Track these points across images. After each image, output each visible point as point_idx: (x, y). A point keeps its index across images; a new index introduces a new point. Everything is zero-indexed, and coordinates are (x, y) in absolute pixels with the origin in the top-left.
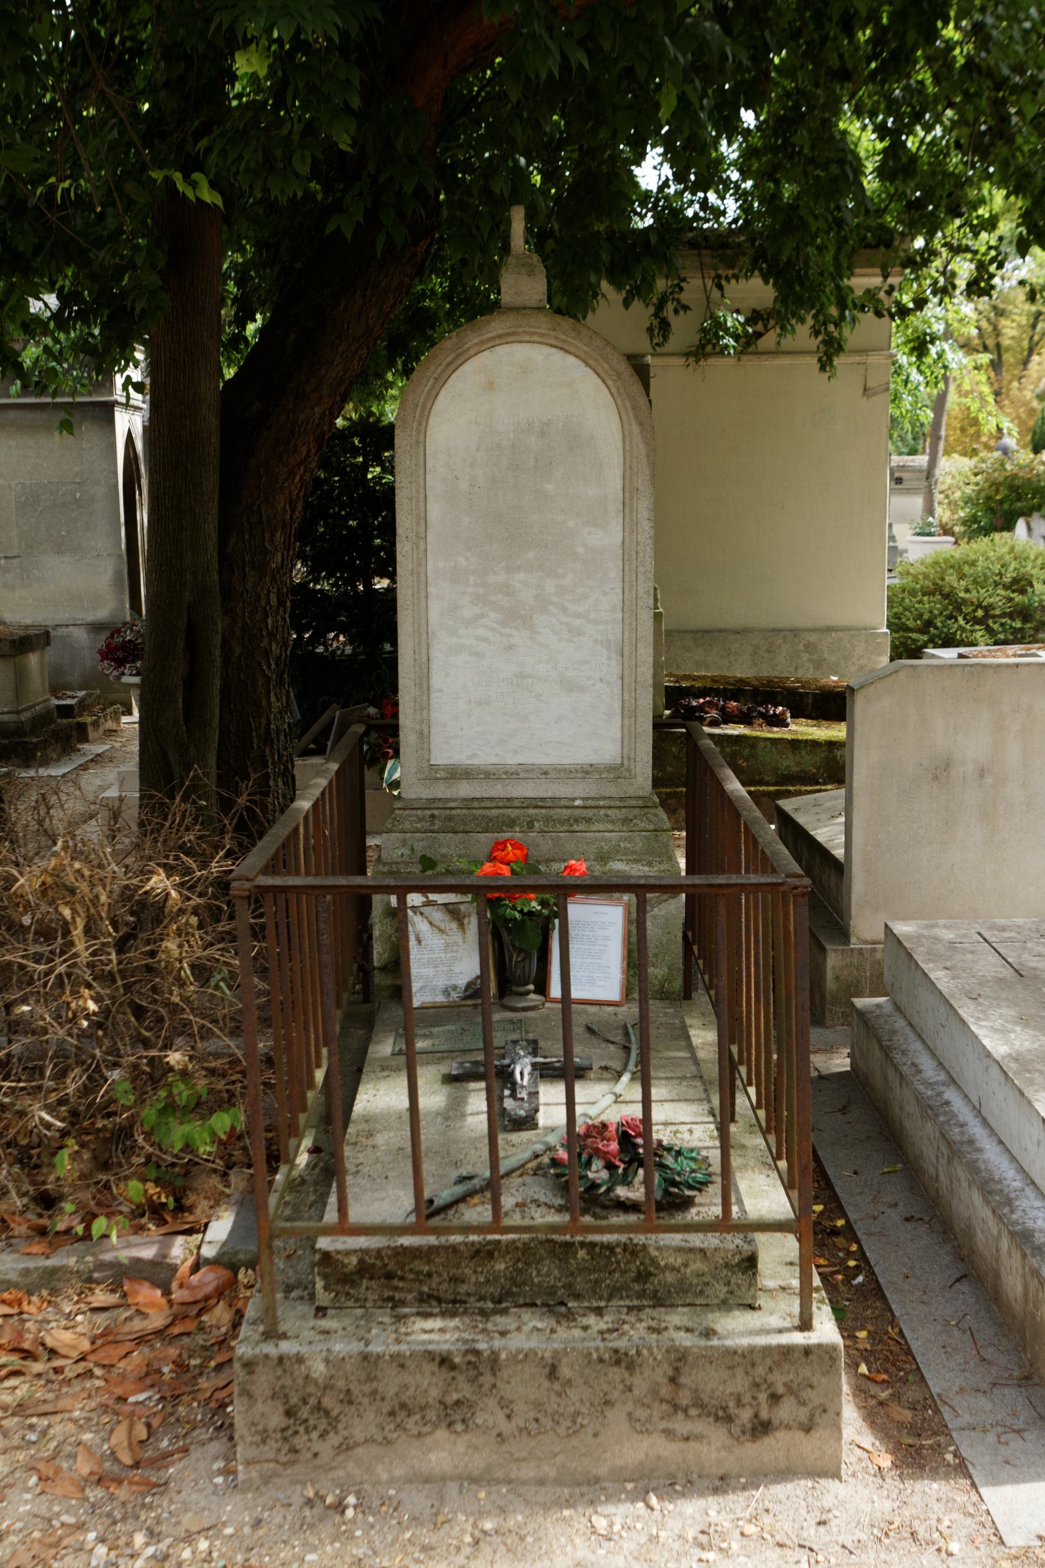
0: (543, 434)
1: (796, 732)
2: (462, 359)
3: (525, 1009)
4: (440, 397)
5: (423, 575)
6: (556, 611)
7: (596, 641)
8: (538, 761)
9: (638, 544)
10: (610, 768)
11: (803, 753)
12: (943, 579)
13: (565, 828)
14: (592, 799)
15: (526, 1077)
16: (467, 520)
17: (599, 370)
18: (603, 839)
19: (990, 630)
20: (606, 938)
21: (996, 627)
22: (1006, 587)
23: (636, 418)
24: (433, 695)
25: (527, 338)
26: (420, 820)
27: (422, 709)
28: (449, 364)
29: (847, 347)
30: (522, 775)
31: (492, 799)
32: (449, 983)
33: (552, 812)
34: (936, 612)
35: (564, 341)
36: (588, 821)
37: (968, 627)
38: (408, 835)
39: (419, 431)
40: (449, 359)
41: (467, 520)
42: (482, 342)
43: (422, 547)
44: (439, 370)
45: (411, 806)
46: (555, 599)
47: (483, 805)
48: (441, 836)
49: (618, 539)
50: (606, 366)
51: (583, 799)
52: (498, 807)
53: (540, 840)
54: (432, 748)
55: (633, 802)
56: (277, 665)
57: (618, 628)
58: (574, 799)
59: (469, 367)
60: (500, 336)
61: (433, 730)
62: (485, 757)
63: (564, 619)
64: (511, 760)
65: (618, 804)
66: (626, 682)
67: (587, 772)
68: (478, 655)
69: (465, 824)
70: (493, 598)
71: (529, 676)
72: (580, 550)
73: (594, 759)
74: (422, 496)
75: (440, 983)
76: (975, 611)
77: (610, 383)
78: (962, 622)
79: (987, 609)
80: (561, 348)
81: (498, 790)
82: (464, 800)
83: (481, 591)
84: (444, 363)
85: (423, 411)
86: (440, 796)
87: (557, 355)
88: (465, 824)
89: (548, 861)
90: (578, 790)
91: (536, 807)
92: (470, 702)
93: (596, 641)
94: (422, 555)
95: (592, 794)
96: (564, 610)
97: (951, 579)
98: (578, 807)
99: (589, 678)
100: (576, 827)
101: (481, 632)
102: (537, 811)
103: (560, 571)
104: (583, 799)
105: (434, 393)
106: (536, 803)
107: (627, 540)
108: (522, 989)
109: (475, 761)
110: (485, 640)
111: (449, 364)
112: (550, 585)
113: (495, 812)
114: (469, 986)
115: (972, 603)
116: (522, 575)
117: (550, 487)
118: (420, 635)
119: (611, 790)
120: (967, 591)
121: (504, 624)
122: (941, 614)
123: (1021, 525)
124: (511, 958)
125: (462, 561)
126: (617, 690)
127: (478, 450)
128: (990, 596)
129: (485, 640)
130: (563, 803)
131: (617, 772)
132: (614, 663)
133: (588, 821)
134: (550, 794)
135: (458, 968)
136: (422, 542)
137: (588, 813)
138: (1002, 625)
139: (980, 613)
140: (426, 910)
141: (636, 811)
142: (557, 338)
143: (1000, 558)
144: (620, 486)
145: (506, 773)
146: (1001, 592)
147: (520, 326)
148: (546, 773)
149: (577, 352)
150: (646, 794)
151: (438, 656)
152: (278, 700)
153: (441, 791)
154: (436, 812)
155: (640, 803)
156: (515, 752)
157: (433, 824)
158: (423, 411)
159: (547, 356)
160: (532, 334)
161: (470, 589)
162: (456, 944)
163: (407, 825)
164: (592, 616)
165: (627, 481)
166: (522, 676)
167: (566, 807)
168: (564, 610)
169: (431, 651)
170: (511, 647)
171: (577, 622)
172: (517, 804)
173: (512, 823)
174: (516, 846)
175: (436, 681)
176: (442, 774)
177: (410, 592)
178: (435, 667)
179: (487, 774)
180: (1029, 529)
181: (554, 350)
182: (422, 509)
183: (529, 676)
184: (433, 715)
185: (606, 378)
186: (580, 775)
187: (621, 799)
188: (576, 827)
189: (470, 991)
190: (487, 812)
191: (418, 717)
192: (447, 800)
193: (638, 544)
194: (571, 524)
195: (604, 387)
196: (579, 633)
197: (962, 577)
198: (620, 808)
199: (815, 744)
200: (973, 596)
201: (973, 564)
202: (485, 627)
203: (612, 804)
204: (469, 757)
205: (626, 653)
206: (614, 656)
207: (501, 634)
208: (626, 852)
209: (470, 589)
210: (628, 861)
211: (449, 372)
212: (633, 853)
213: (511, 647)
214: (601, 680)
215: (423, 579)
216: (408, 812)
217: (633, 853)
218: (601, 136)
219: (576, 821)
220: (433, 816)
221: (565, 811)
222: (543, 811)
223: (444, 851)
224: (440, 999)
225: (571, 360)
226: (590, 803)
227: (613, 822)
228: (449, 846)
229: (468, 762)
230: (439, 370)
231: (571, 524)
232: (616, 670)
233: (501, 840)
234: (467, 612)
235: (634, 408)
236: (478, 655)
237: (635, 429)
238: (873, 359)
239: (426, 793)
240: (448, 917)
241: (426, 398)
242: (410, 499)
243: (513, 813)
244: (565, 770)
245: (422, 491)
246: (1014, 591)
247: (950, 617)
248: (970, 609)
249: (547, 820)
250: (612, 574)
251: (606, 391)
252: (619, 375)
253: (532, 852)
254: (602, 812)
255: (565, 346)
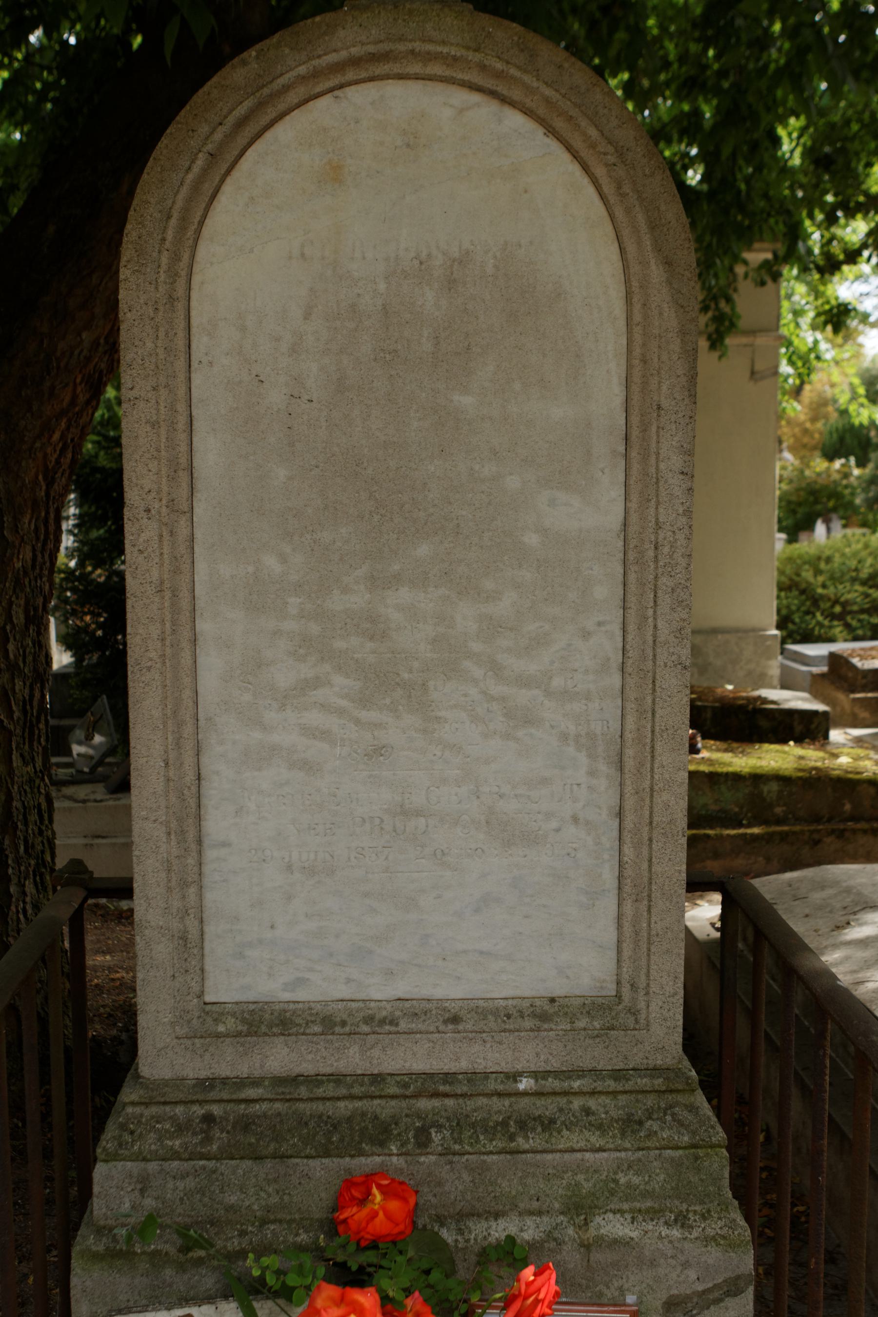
0: (451, 284)
1: (710, 762)
2: (271, 113)
4: (224, 199)
5: (185, 594)
6: (478, 673)
7: (564, 737)
8: (439, 993)
9: (658, 526)
10: (593, 1007)
11: (723, 788)
12: (798, 575)
13: (498, 1144)
14: (557, 1074)
16: (282, 473)
17: (578, 143)
19: (847, 626)
21: (854, 623)
22: (864, 583)
23: (658, 249)
24: (210, 854)
25: (416, 68)
26: (181, 1128)
27: (184, 884)
28: (241, 123)
29: (742, 324)
30: (403, 1025)
31: (337, 1078)
33: (470, 1104)
34: (794, 608)
35: (499, 75)
36: (548, 1125)
37: (826, 623)
39: (173, 275)
40: (241, 111)
41: (282, 473)
42: (316, 75)
43: (183, 531)
44: (218, 136)
45: (159, 1094)
46: (476, 646)
47: (320, 1092)
48: (225, 1166)
49: (615, 518)
50: (593, 132)
51: (535, 1075)
52: (352, 1097)
54: (208, 967)
55: (644, 1082)
56: (24, 712)
57: (612, 708)
58: (515, 1077)
59: (284, 133)
60: (355, 62)
61: (209, 929)
62: (325, 984)
63: (496, 689)
64: (380, 990)
65: (611, 1085)
66: (629, 824)
67: (544, 1017)
68: (309, 767)
70: (340, 644)
71: (418, 813)
72: (532, 539)
73: (558, 987)
74: (182, 420)
76: (833, 606)
77: (600, 172)
78: (819, 617)
79: (845, 604)
80: (492, 94)
81: (351, 1059)
82: (279, 1081)
83: (314, 628)
84: (231, 120)
85: (182, 228)
86: (224, 1071)
87: (484, 110)
89: (461, 1217)
90: (523, 1055)
91: (436, 1095)
92: (289, 868)
93: (564, 737)
94: (182, 549)
95: (555, 1064)
96: (496, 669)
97: (807, 575)
98: (525, 1094)
99: (549, 815)
101: (314, 718)
102: (436, 1103)
103: (489, 585)
104: (535, 1075)
105: (207, 188)
106: (434, 1084)
107: (634, 518)
109: (302, 995)
110: (324, 735)
111: (241, 123)
112: (466, 616)
113: (344, 1107)
115: (829, 599)
116: (404, 595)
117: (466, 401)
118: (180, 724)
119: (598, 1056)
120: (824, 586)
121: (364, 702)
122: (798, 609)
123: (820, 528)
125: (271, 562)
126: (609, 838)
127: (307, 316)
128: (849, 592)
129: (324, 735)
130: (492, 1085)
131: (607, 1013)
132: (602, 783)
133: (548, 1125)
134: (464, 1065)
136: (183, 521)
137: (547, 1107)
138: (859, 621)
139: (838, 609)
141: (650, 1101)
142: (483, 68)
143: (855, 554)
144: (618, 401)
145: (369, 1020)
146: (858, 587)
147: (401, 39)
148: (455, 1020)
149: (529, 103)
150: (669, 1061)
151: (221, 775)
152: (25, 763)
153: (228, 1062)
154: (216, 1110)
155: (658, 1082)
156: (389, 973)
158: (182, 228)
159: (461, 111)
160: (429, 58)
161: (290, 625)
163: (150, 1143)
164: (557, 682)
165: (635, 389)
166: (405, 812)
167: (500, 1095)
168: (496, 669)
169: (204, 760)
170: (379, 751)
171: (523, 696)
172: (393, 1090)
173: (381, 1133)
175: (216, 824)
176: (230, 1024)
177: (155, 631)
178: (212, 793)
179: (329, 1023)
180: (829, 530)
181: (476, 98)
182: (183, 448)
183: (418, 813)
184: (209, 896)
185: (592, 161)
186: (528, 1023)
187: (618, 1075)
188: (520, 1142)
190: (327, 1108)
191: (176, 904)
192: (242, 1083)
193: (658, 526)
194: (513, 482)
195: (585, 181)
196: (529, 719)
197: (818, 572)
198: (614, 1094)
199: (737, 777)
200: (831, 591)
201: (829, 560)
202: (324, 707)
203: (599, 1086)
204: (286, 987)
205: (630, 763)
206: (603, 767)
207: (357, 722)
209: (290, 625)
211: (241, 140)
212: (646, 1194)
213: (379, 751)
214: (575, 819)
215: (185, 604)
216: (154, 1110)
217: (646, 1194)
219: (523, 1125)
220: (209, 1119)
221: (496, 1103)
222: (450, 1102)
225: (515, 120)
226: (551, 1083)
227: (600, 1127)
228: (242, 1189)
229: (287, 996)
230: (218, 136)
231: (513, 482)
232: (608, 798)
234: (284, 675)
235: (653, 227)
236: (309, 767)
237: (656, 272)
238: (761, 341)
239: (195, 1068)
241: (189, 200)
242: (155, 425)
243: (385, 1109)
244: (496, 1012)
245: (181, 407)
246: (871, 587)
247: (807, 613)
248: (828, 604)
249: (459, 1124)
250: (600, 592)
251: (591, 190)
252: (621, 152)
254: (577, 1103)
255: (501, 89)
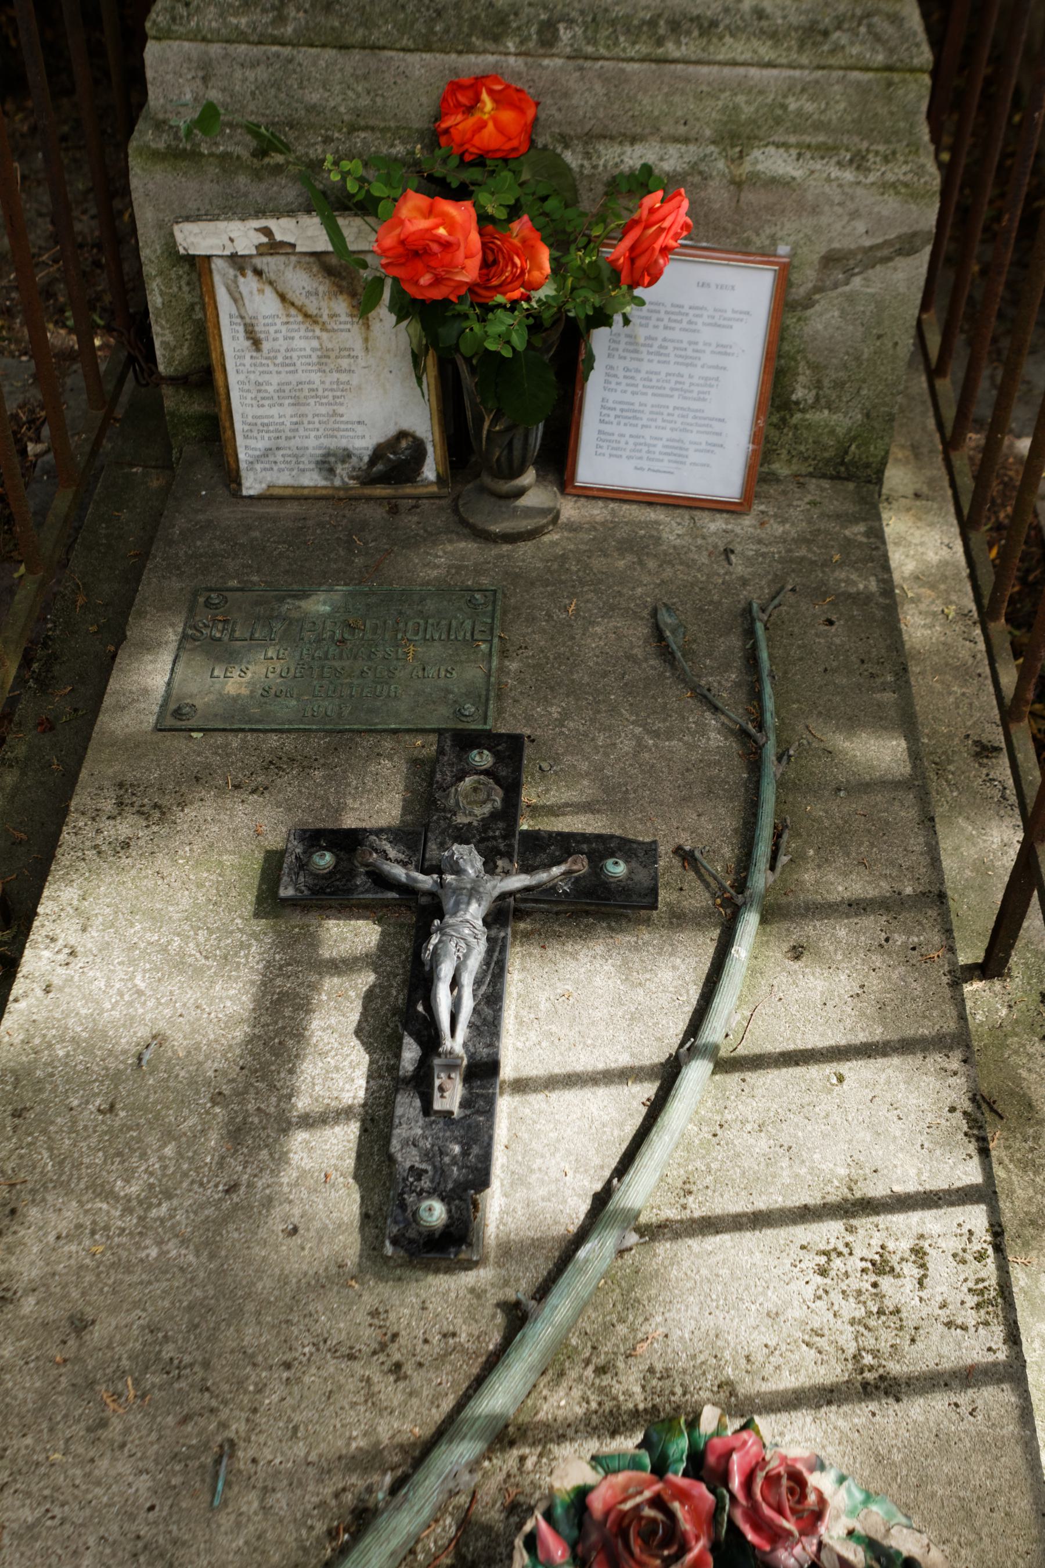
3: (511, 538)
15: (462, 1031)
18: (742, 86)
20: (723, 349)
32: (333, 444)
38: (215, 49)
48: (305, 55)
53: (572, 81)
69: (367, 23)
75: (311, 443)
88: (367, 23)
89: (591, 138)
100: (671, 49)
108: (506, 486)
114: (378, 453)
124: (479, 420)
135: (351, 411)
140: (270, 264)
157: (281, 19)
162: (346, 351)
174: (509, 98)
188: (671, 49)
189: (380, 467)
208: (801, 123)
210: (803, 150)
212: (819, 126)
217: (819, 126)
218: (350, 1496)
223: (314, 97)
224: (312, 479)
227: (774, 36)
228: (325, 85)
233: (465, 78)
240: (323, 286)
253: (550, 111)
